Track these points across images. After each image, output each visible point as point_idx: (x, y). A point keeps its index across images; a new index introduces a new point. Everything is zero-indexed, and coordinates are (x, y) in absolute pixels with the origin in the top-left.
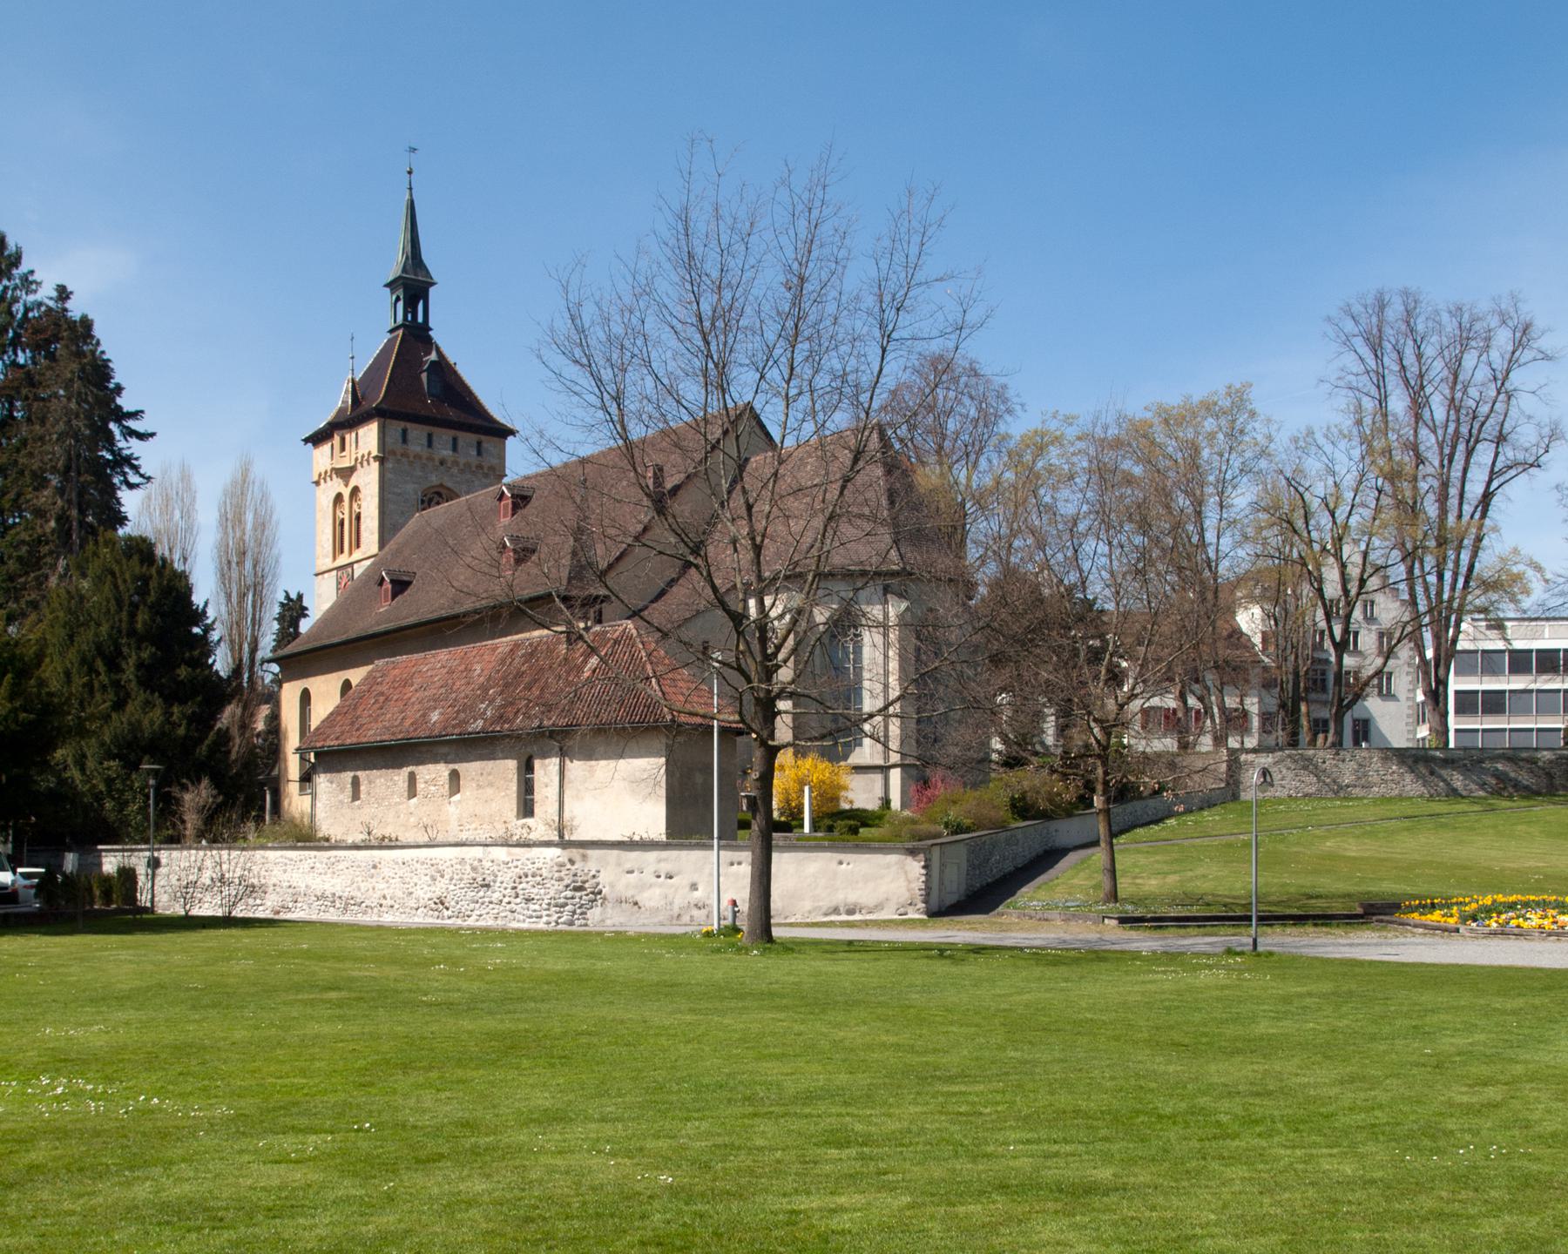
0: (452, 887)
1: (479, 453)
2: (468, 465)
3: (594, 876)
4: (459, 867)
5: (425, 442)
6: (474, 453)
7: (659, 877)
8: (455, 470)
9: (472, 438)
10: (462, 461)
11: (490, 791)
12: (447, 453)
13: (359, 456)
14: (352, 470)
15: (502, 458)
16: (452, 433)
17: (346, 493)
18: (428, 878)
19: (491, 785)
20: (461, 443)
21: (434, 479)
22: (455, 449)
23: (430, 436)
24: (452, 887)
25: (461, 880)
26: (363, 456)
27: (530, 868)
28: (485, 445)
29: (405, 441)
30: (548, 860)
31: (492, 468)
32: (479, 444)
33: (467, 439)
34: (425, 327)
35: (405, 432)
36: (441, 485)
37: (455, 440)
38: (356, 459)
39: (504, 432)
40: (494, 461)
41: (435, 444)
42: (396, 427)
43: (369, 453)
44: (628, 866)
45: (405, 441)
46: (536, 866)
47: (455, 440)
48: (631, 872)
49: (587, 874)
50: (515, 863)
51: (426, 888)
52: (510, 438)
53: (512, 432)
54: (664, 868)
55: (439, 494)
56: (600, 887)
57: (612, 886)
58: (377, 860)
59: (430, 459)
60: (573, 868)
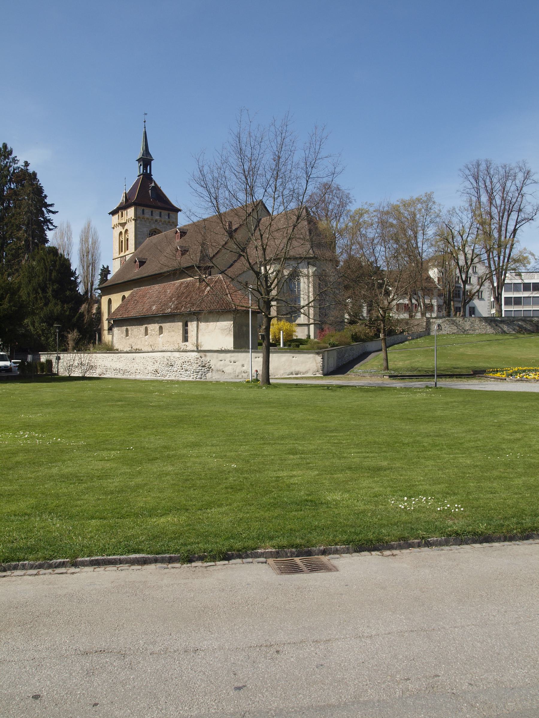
0: (160, 366)
1: (169, 218)
2: (165, 221)
7: (231, 362)
8: (160, 223)
10: (163, 220)
11: (173, 333)
12: (158, 217)
13: (128, 219)
14: (125, 223)
15: (177, 219)
17: (123, 232)
18: (152, 363)
19: (173, 331)
20: (162, 214)
21: (153, 226)
22: (160, 216)
23: (152, 212)
24: (160, 366)
25: (163, 363)
26: (129, 219)
27: (187, 360)
28: (171, 215)
29: (143, 213)
30: (193, 357)
31: (173, 223)
32: (169, 214)
34: (150, 175)
35: (143, 210)
37: (160, 213)
39: (178, 210)
40: (174, 220)
41: (153, 214)
42: (140, 209)
43: (131, 218)
44: (220, 359)
45: (143, 213)
46: (189, 358)
47: (160, 213)
48: (221, 361)
49: (206, 362)
50: (182, 358)
51: (151, 366)
52: (179, 213)
53: (180, 210)
54: (233, 359)
55: (155, 232)
56: (211, 366)
58: (134, 357)
59: (152, 219)
60: (202, 359)
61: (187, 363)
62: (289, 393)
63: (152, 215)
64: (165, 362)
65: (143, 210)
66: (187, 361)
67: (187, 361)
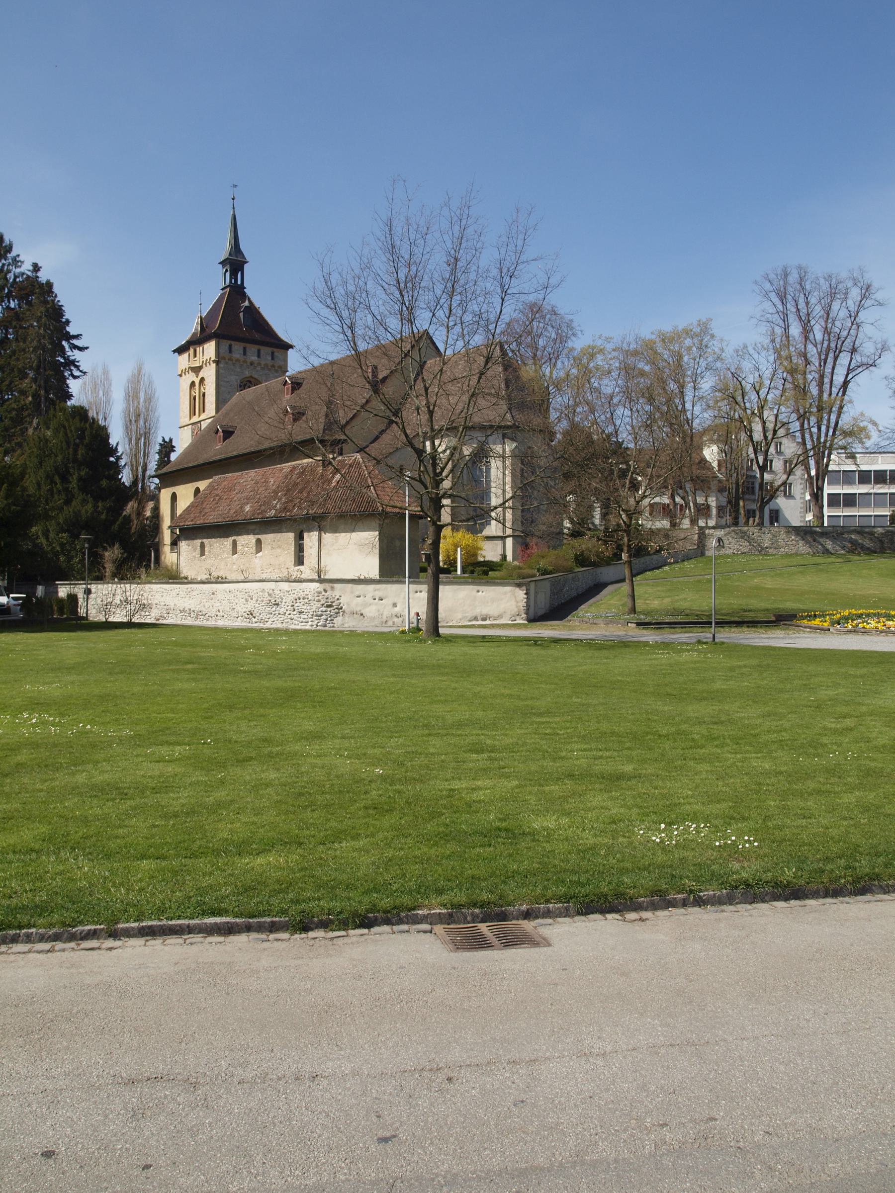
0: (257, 605)
1: (273, 359)
2: (266, 365)
3: (338, 599)
4: (261, 593)
5: (242, 352)
6: (270, 358)
7: (375, 599)
8: (259, 368)
9: (269, 350)
10: (263, 363)
11: (279, 551)
12: (254, 358)
13: (205, 360)
14: (200, 368)
15: (286, 361)
16: (257, 347)
17: (197, 381)
19: (279, 547)
20: (262, 352)
21: (247, 373)
22: (259, 356)
23: (245, 349)
24: (257, 605)
25: (262, 601)
26: (207, 360)
27: (301, 594)
28: (276, 354)
29: (230, 351)
30: (312, 590)
31: (280, 367)
32: (273, 353)
33: (266, 350)
34: (242, 287)
35: (230, 346)
36: (251, 377)
37: (259, 351)
38: (203, 362)
39: (288, 347)
40: (281, 363)
41: (248, 353)
42: (225, 344)
43: (210, 359)
44: (357, 593)
45: (230, 351)
46: (305, 593)
47: (259, 351)
50: (293, 592)
51: (243, 606)
52: (290, 350)
53: (291, 347)
54: (378, 594)
57: (348, 604)
59: (245, 362)
61: (301, 600)
62: (469, 650)
63: (245, 353)
64: (265, 599)
65: (230, 346)
66: (301, 597)
67: (301, 597)
